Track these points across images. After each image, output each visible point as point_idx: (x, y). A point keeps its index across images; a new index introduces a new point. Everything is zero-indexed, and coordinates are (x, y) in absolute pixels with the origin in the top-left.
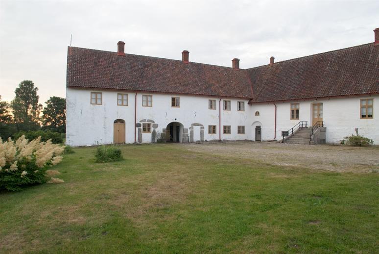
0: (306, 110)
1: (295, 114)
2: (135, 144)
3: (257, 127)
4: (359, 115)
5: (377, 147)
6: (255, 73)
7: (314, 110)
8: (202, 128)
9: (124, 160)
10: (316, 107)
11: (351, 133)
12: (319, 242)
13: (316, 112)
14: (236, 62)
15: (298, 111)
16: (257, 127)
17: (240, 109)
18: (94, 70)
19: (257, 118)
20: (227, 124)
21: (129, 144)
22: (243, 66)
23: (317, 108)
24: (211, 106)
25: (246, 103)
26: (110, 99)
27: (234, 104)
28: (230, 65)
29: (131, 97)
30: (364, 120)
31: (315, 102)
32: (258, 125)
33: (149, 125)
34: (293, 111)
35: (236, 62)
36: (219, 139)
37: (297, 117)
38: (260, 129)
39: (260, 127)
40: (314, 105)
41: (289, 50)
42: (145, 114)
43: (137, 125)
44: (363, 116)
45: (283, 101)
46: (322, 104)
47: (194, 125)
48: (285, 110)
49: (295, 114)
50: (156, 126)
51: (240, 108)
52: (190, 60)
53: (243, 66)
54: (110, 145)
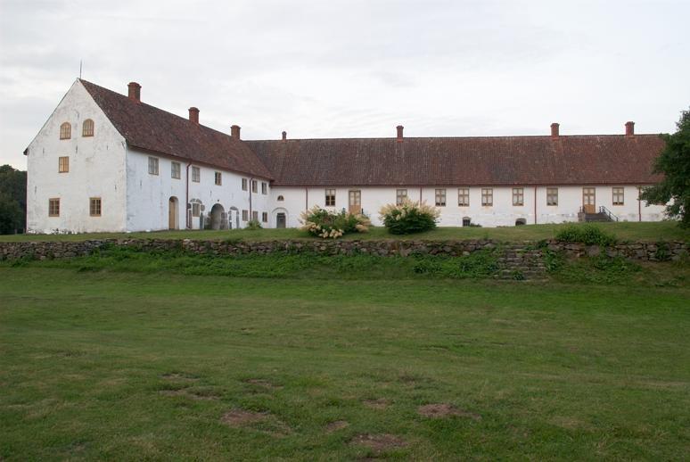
1: (330, 201)
2: (186, 230)
3: (279, 214)
5: (663, 254)
6: (258, 147)
8: (238, 213)
10: (352, 194)
14: (236, 129)
15: (333, 198)
16: (279, 214)
19: (281, 204)
21: (182, 231)
22: (244, 137)
24: (244, 187)
26: (165, 166)
29: (183, 167)
31: (354, 189)
32: (282, 211)
33: (198, 205)
34: (327, 198)
35: (236, 129)
36: (166, 226)
37: (333, 204)
38: (284, 217)
39: (283, 214)
41: (305, 128)
43: (188, 206)
45: (317, 186)
47: (231, 208)
49: (330, 201)
51: (264, 191)
52: (636, 132)
53: (244, 137)
54: (166, 231)
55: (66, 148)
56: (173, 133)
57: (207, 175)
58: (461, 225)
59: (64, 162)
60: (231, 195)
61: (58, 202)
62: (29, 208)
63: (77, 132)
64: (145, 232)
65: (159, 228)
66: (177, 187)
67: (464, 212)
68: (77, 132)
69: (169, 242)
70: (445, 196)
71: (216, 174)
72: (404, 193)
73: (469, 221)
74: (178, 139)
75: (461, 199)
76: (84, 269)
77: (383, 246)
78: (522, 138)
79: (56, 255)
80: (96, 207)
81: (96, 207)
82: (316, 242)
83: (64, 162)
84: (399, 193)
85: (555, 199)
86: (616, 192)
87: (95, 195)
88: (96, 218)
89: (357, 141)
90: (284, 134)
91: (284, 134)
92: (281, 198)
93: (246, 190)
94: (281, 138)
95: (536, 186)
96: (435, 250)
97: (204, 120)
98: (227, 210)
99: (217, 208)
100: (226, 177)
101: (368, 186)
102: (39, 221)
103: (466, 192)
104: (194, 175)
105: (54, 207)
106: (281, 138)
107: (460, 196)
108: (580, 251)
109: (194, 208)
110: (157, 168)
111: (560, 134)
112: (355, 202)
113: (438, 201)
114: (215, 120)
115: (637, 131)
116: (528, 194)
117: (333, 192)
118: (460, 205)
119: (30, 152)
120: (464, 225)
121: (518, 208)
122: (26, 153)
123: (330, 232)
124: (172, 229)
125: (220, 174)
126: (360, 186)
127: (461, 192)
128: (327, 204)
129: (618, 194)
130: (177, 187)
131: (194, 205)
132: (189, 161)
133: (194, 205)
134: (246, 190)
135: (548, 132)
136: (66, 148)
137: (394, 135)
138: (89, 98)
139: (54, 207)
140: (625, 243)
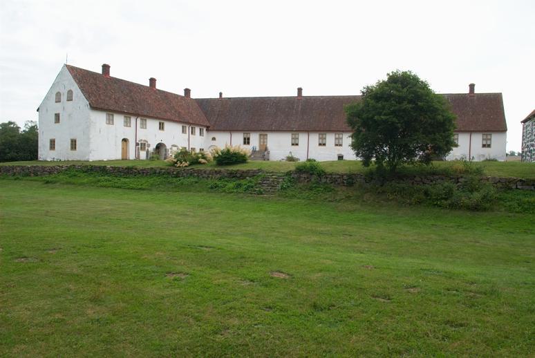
0: (255, 139)
1: (247, 141)
4: (318, 144)
6: (202, 103)
7: (260, 138)
9: (248, 163)
10: (262, 137)
11: (288, 154)
12: (532, 148)
13: (262, 140)
15: (249, 139)
17: (200, 135)
18: (105, 92)
19: (214, 143)
20: (193, 147)
22: (193, 96)
23: (263, 138)
24: (184, 131)
25: (205, 130)
26: (119, 119)
27: (197, 130)
28: (182, 94)
29: (133, 120)
30: (293, 147)
33: (145, 144)
34: (245, 139)
35: (187, 91)
36: (119, 157)
37: (248, 143)
40: (260, 135)
41: (234, 91)
42: (143, 135)
43: (137, 144)
44: (293, 144)
45: (237, 131)
46: (267, 135)
47: (173, 146)
48: (286, 138)
49: (247, 141)
50: (149, 146)
51: (201, 134)
53: (193, 96)
55: (58, 108)
56: (131, 97)
57: (153, 125)
58: (336, 159)
59: (57, 117)
60: (175, 138)
61: (54, 141)
62: (39, 145)
63: (64, 98)
64: (103, 161)
65: (113, 158)
66: (129, 133)
67: (339, 150)
68: (64, 98)
69: (100, 167)
70: (325, 139)
71: (160, 124)
72: (297, 136)
73: (342, 157)
74: (133, 101)
75: (337, 141)
76: (47, 182)
77: (205, 172)
78: (334, 97)
79: (39, 173)
80: (74, 144)
81: (74, 144)
82: (172, 168)
83: (57, 117)
84: (294, 136)
85: (340, 141)
86: (294, 136)
87: (73, 137)
88: (74, 152)
89: (269, 99)
90: (472, 87)
91: (472, 87)
92: (214, 139)
93: (185, 133)
94: (218, 97)
95: (471, 132)
96: (232, 175)
97: (159, 86)
98: (168, 147)
99: (159, 147)
100: (167, 125)
101: (272, 131)
102: (45, 154)
103: (341, 136)
104: (142, 124)
105: (52, 143)
106: (218, 97)
107: (336, 139)
108: (308, 178)
109: (142, 146)
110: (113, 120)
111: (468, 92)
112: (264, 142)
113: (321, 142)
114: (171, 84)
115: (477, 91)
116: (303, 138)
117: (248, 136)
118: (336, 145)
119: (40, 110)
120: (339, 159)
121: (486, 149)
122: (38, 110)
123: (181, 163)
124: (125, 159)
125: (163, 123)
126: (343, 131)
127: (337, 136)
128: (245, 143)
129: (487, 140)
130: (129, 133)
131: (141, 144)
132: (137, 115)
133: (141, 144)
134: (185, 133)
135: (295, 94)
136: (58, 108)
137: (467, 91)
138: (70, 77)
139: (52, 143)
140: (331, 174)
